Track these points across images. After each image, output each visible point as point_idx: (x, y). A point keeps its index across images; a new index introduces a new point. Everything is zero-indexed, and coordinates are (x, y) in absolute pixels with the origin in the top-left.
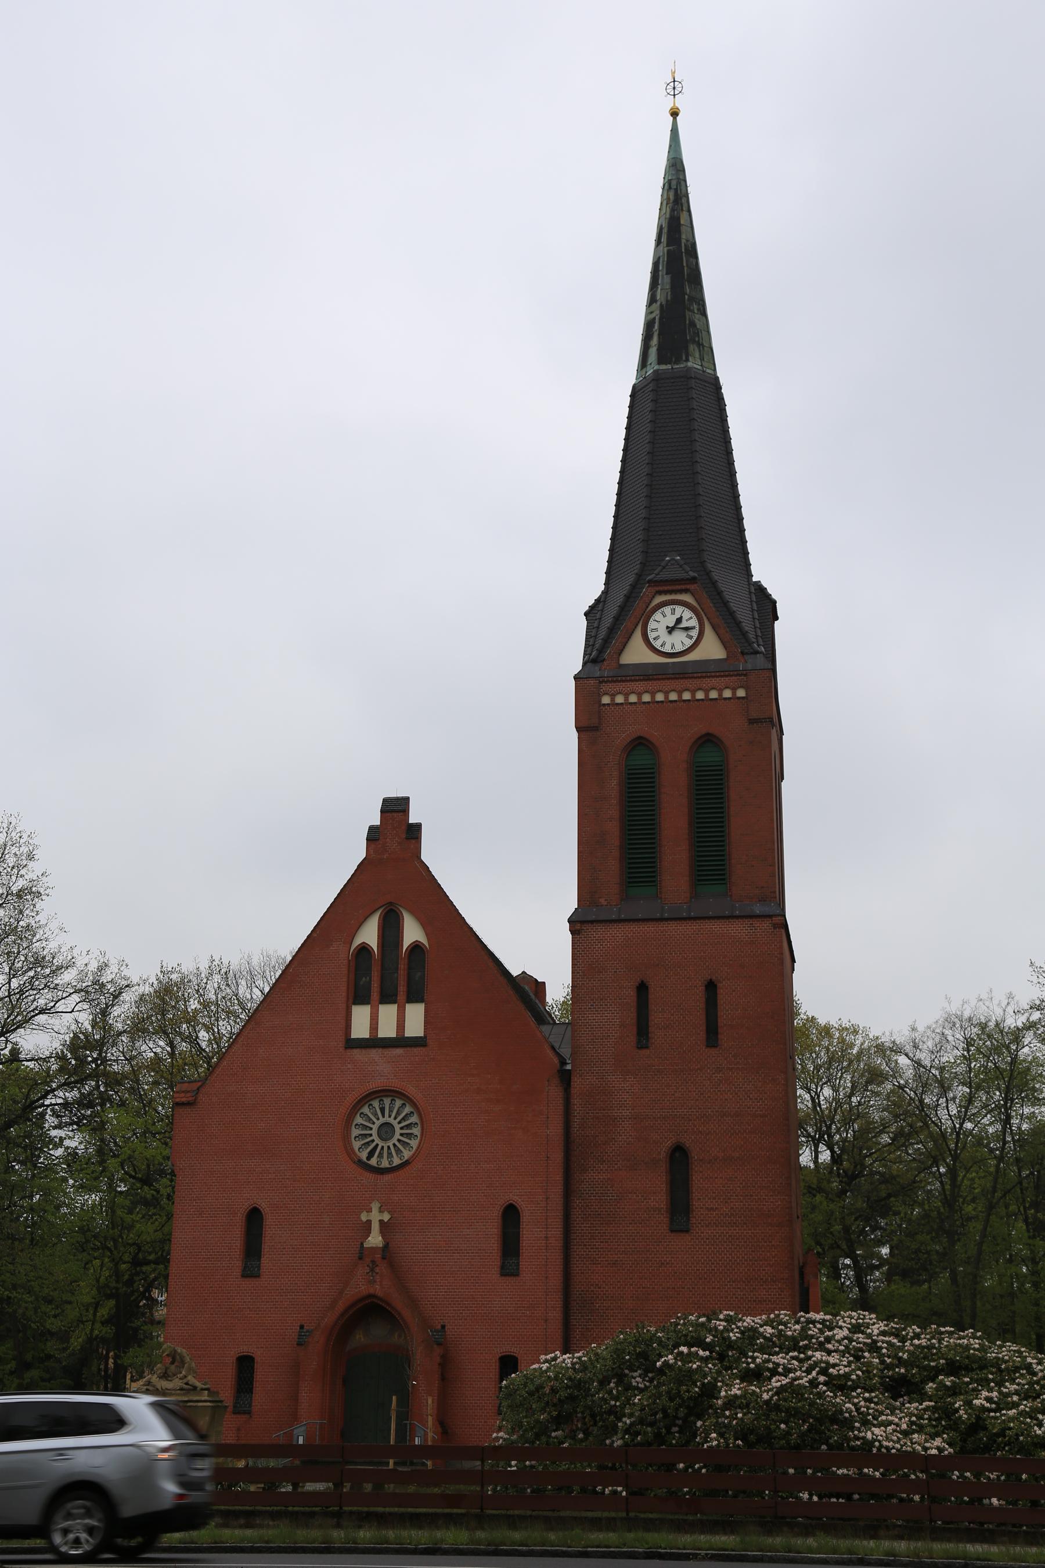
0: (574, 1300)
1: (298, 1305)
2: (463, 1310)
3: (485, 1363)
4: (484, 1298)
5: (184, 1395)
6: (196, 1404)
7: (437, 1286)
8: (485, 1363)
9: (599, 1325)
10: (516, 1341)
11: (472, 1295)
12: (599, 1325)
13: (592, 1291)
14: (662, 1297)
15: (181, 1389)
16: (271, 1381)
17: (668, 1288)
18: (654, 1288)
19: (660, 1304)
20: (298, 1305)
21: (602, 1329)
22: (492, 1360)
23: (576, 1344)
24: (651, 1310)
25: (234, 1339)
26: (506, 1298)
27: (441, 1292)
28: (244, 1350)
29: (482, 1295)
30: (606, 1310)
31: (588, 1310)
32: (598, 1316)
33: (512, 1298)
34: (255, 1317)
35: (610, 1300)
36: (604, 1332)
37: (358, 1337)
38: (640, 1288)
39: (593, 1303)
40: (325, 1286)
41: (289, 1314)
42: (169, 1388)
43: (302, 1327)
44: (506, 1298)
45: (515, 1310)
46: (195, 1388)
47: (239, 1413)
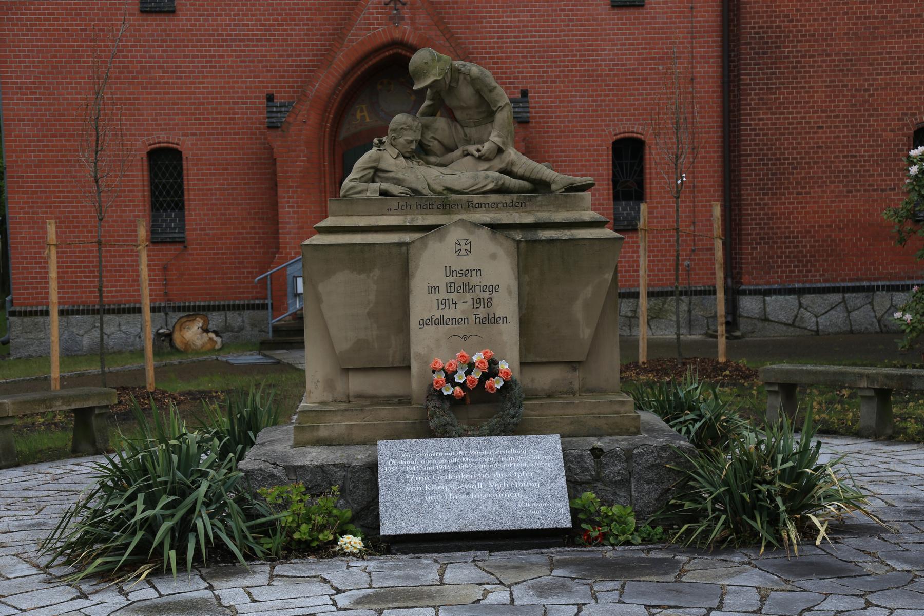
0: (746, 44)
1: (253, 61)
2: (549, 67)
3: (589, 151)
4: (583, 46)
5: (513, 206)
6: (566, 234)
7: (502, 27)
8: (589, 151)
9: (789, 83)
10: (642, 114)
11: (564, 41)
12: (789, 83)
13: (777, 27)
14: (899, 32)
15: (501, 190)
16: (217, 190)
17: (910, 16)
18: (886, 17)
19: (896, 43)
20: (253, 61)
21: (793, 88)
22: (601, 146)
23: (750, 115)
24: (879, 54)
25: (138, 120)
26: (622, 44)
27: (508, 37)
28: (162, 138)
29: (580, 41)
30: (802, 57)
31: (771, 58)
32: (788, 68)
33: (632, 44)
34: (174, 83)
35: (809, 41)
36: (797, 93)
37: (359, 115)
38: (860, 18)
39: (779, 47)
40: (300, 30)
41: (238, 77)
42: (457, 187)
43: (270, 98)
44: (622, 44)
45: (639, 64)
46: (540, 186)
47: (163, 242)
